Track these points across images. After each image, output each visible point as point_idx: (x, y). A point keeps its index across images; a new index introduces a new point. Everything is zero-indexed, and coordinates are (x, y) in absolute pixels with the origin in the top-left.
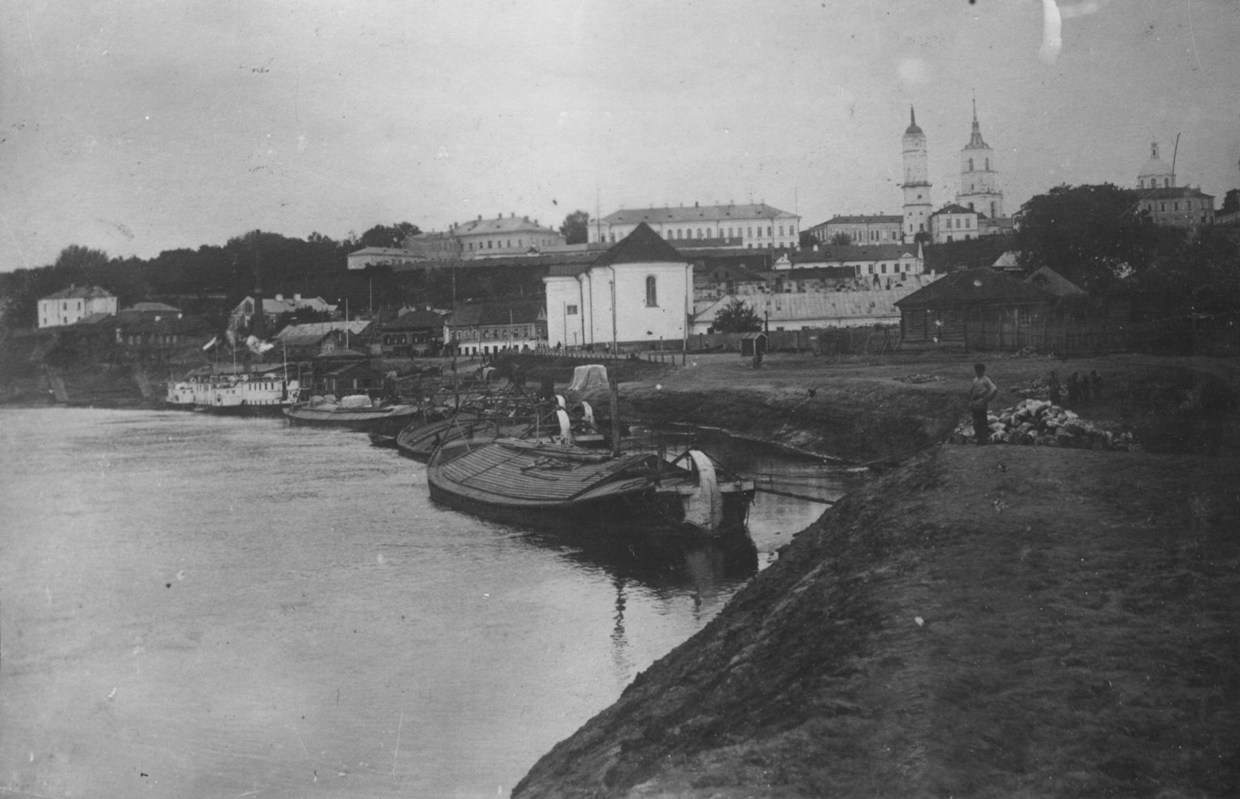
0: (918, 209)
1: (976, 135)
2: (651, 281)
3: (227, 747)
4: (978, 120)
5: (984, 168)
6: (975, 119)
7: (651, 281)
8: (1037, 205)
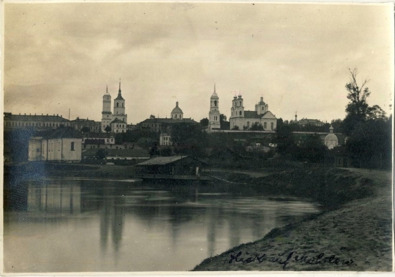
0: (106, 121)
1: (120, 95)
2: (73, 144)
3: (279, 242)
4: (121, 90)
5: (122, 106)
6: (120, 89)
7: (73, 144)
8: (201, 121)
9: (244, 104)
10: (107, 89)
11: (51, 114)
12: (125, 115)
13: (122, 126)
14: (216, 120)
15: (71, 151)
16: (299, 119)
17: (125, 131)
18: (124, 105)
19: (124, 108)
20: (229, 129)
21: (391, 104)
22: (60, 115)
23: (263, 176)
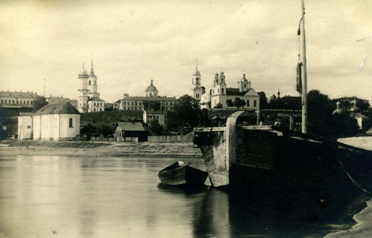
2: (71, 120)
9: (226, 81)
10: (84, 65)
11: (25, 91)
13: (100, 104)
16: (282, 96)
18: (96, 83)
21: (27, 127)
22: (34, 92)
23: (235, 151)
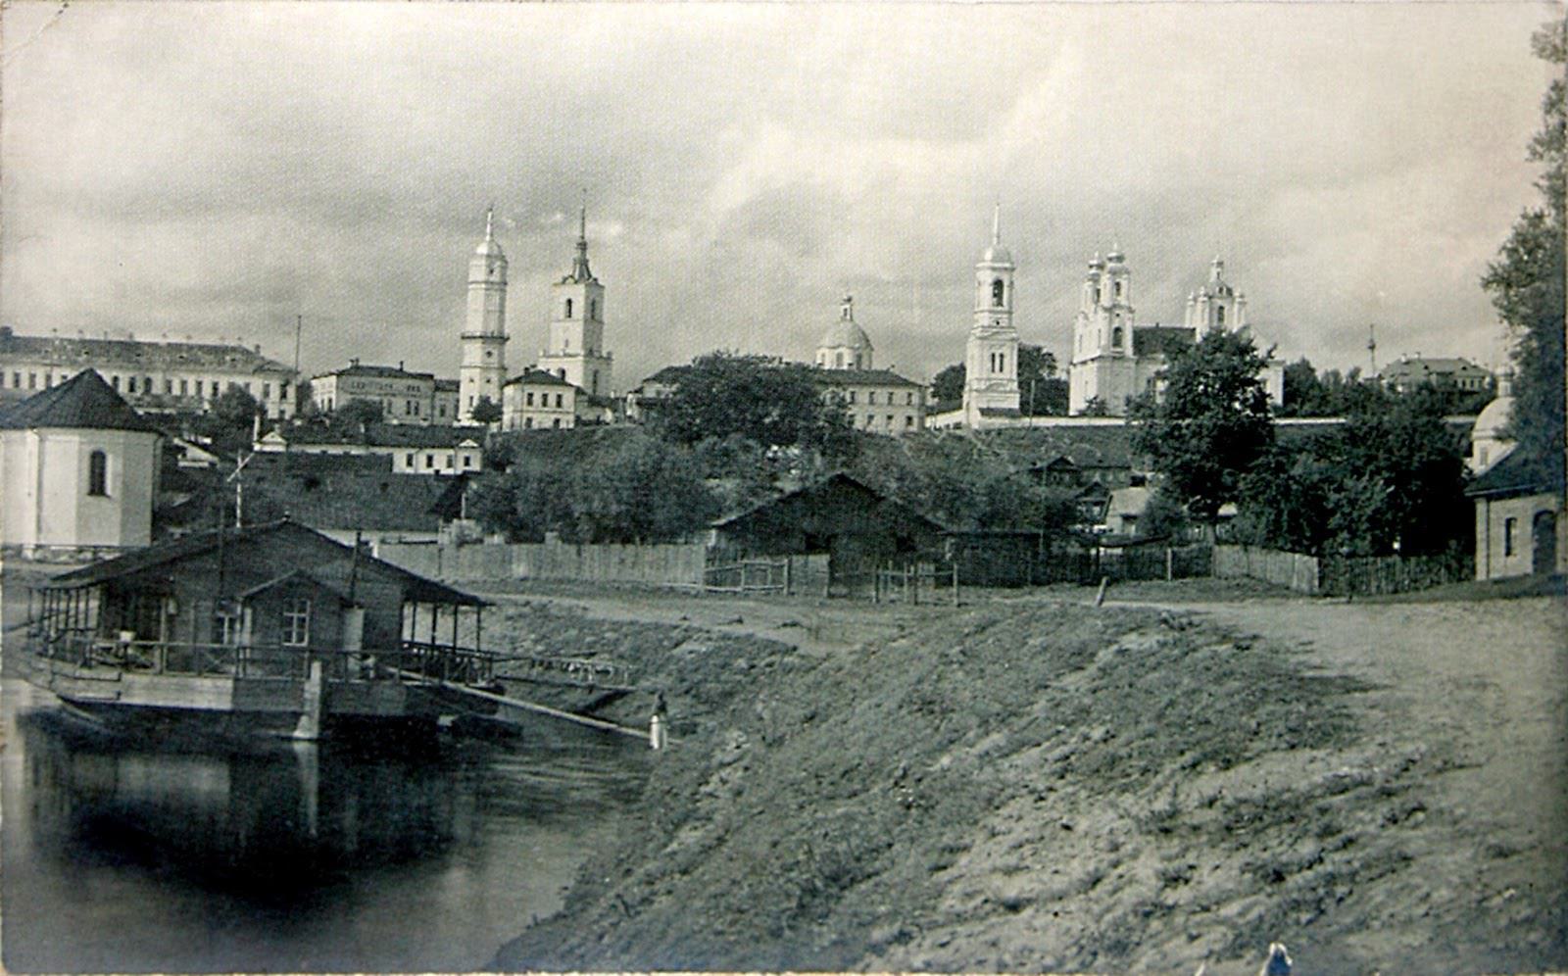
2: (98, 460)
12: (604, 354)
13: (552, 400)
14: (1001, 370)
15: (90, 499)
17: (567, 423)
19: (601, 323)
20: (1066, 415)
